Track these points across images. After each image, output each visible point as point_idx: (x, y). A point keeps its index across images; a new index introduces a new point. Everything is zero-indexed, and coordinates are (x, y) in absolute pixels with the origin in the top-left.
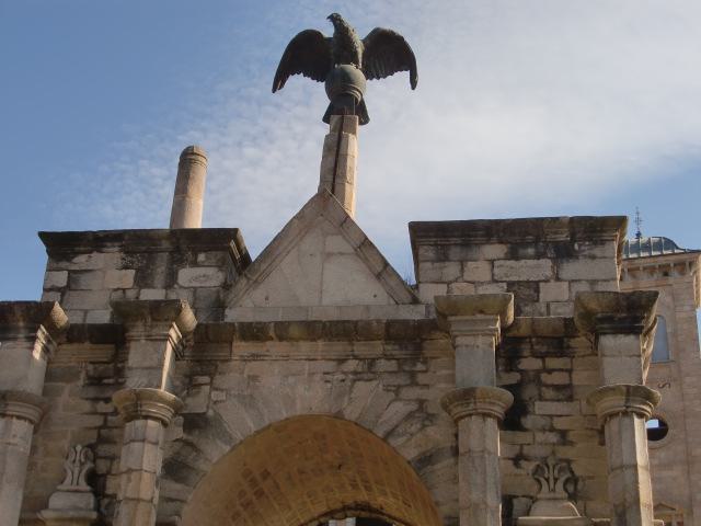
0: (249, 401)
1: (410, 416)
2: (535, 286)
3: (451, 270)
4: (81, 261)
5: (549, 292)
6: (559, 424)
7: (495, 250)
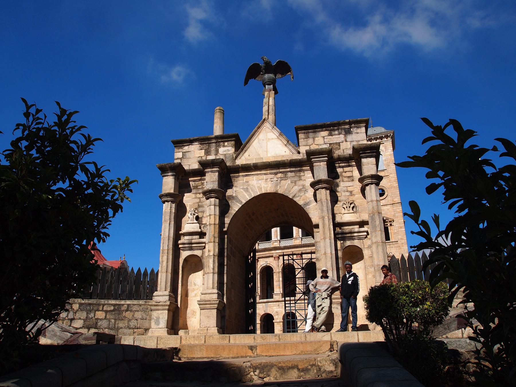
0: (247, 190)
1: (300, 191)
2: (339, 144)
3: (310, 141)
4: (186, 148)
5: (343, 146)
6: (350, 189)
7: (325, 133)
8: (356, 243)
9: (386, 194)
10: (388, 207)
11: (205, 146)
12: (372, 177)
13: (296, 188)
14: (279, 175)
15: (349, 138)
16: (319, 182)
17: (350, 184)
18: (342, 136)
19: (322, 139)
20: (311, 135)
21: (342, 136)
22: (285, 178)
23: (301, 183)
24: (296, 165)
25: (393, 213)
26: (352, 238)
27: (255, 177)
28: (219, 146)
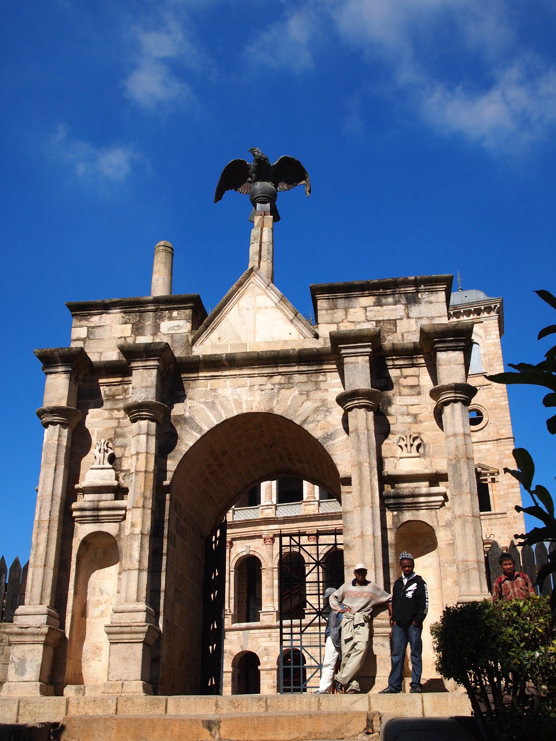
0: (212, 406)
1: (316, 410)
2: (394, 322)
4: (95, 320)
5: (402, 326)
7: (367, 301)
8: (423, 515)
9: (485, 419)
10: (489, 445)
11: (134, 318)
12: (457, 388)
13: (309, 406)
14: (277, 379)
15: (415, 311)
16: (354, 395)
17: (414, 400)
18: (401, 308)
19: (361, 312)
20: (341, 303)
21: (401, 308)
22: (289, 385)
23: (319, 395)
24: (310, 360)
25: (497, 458)
26: (415, 507)
27: (229, 381)
28: (161, 318)
